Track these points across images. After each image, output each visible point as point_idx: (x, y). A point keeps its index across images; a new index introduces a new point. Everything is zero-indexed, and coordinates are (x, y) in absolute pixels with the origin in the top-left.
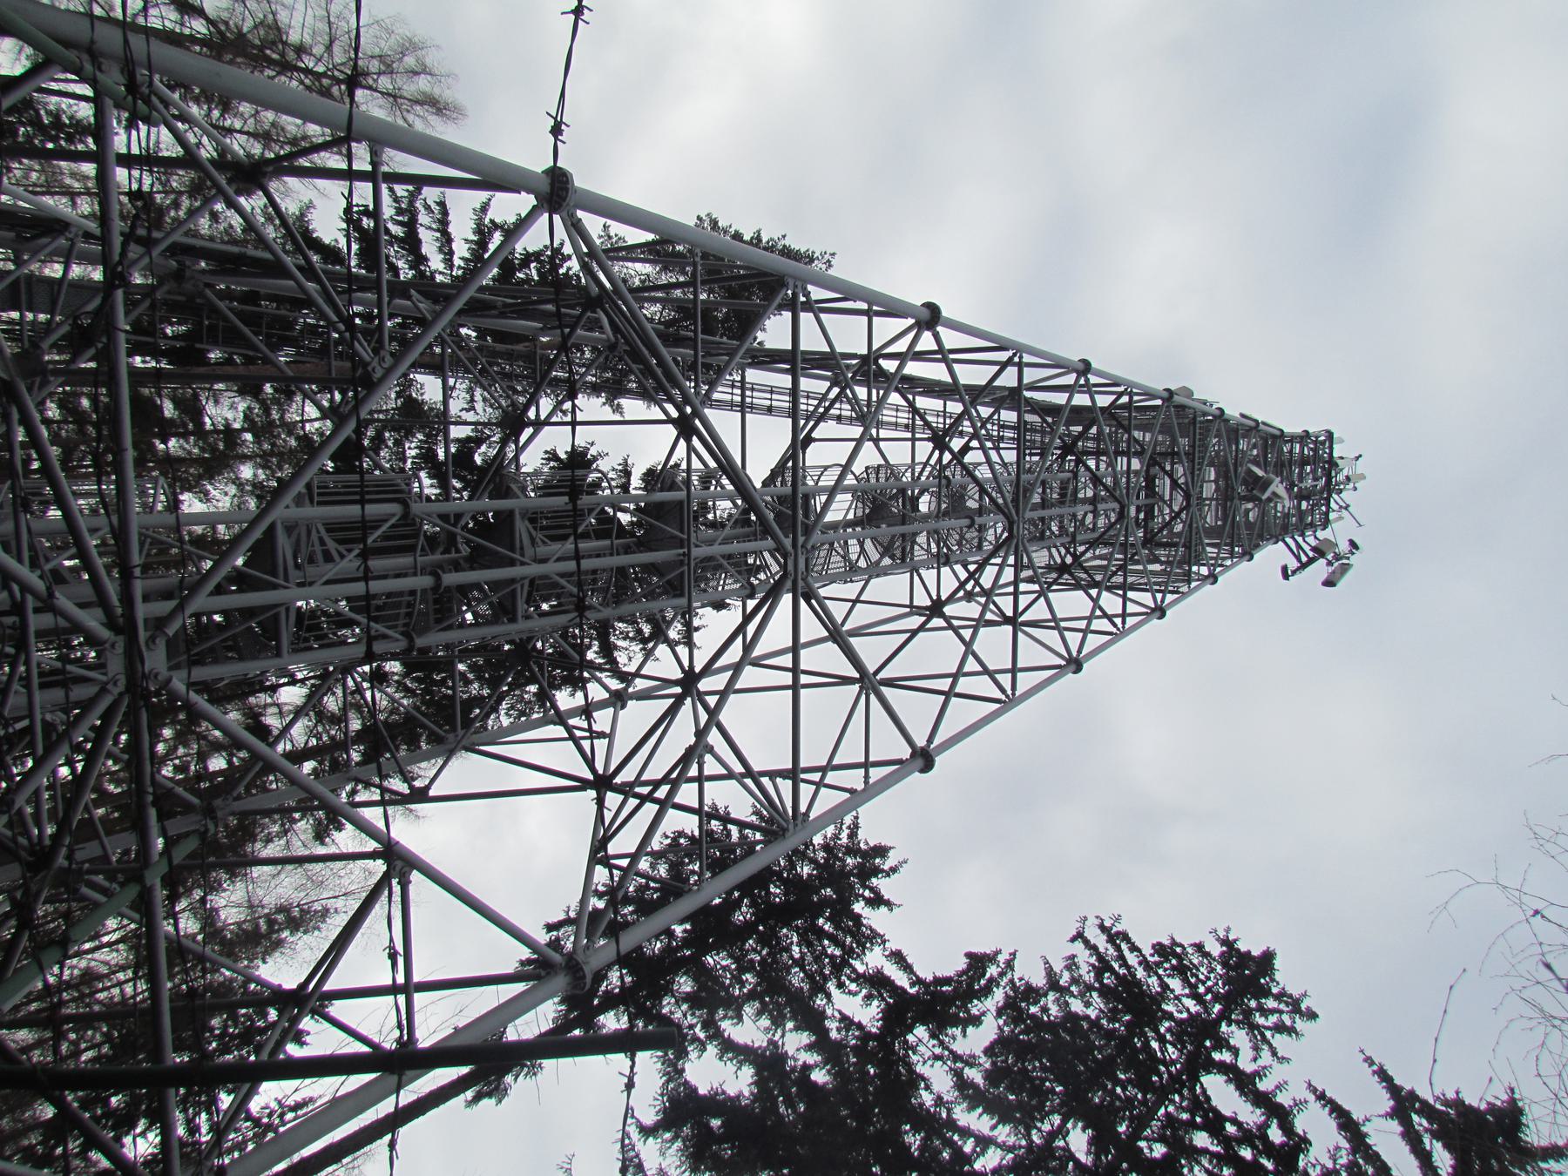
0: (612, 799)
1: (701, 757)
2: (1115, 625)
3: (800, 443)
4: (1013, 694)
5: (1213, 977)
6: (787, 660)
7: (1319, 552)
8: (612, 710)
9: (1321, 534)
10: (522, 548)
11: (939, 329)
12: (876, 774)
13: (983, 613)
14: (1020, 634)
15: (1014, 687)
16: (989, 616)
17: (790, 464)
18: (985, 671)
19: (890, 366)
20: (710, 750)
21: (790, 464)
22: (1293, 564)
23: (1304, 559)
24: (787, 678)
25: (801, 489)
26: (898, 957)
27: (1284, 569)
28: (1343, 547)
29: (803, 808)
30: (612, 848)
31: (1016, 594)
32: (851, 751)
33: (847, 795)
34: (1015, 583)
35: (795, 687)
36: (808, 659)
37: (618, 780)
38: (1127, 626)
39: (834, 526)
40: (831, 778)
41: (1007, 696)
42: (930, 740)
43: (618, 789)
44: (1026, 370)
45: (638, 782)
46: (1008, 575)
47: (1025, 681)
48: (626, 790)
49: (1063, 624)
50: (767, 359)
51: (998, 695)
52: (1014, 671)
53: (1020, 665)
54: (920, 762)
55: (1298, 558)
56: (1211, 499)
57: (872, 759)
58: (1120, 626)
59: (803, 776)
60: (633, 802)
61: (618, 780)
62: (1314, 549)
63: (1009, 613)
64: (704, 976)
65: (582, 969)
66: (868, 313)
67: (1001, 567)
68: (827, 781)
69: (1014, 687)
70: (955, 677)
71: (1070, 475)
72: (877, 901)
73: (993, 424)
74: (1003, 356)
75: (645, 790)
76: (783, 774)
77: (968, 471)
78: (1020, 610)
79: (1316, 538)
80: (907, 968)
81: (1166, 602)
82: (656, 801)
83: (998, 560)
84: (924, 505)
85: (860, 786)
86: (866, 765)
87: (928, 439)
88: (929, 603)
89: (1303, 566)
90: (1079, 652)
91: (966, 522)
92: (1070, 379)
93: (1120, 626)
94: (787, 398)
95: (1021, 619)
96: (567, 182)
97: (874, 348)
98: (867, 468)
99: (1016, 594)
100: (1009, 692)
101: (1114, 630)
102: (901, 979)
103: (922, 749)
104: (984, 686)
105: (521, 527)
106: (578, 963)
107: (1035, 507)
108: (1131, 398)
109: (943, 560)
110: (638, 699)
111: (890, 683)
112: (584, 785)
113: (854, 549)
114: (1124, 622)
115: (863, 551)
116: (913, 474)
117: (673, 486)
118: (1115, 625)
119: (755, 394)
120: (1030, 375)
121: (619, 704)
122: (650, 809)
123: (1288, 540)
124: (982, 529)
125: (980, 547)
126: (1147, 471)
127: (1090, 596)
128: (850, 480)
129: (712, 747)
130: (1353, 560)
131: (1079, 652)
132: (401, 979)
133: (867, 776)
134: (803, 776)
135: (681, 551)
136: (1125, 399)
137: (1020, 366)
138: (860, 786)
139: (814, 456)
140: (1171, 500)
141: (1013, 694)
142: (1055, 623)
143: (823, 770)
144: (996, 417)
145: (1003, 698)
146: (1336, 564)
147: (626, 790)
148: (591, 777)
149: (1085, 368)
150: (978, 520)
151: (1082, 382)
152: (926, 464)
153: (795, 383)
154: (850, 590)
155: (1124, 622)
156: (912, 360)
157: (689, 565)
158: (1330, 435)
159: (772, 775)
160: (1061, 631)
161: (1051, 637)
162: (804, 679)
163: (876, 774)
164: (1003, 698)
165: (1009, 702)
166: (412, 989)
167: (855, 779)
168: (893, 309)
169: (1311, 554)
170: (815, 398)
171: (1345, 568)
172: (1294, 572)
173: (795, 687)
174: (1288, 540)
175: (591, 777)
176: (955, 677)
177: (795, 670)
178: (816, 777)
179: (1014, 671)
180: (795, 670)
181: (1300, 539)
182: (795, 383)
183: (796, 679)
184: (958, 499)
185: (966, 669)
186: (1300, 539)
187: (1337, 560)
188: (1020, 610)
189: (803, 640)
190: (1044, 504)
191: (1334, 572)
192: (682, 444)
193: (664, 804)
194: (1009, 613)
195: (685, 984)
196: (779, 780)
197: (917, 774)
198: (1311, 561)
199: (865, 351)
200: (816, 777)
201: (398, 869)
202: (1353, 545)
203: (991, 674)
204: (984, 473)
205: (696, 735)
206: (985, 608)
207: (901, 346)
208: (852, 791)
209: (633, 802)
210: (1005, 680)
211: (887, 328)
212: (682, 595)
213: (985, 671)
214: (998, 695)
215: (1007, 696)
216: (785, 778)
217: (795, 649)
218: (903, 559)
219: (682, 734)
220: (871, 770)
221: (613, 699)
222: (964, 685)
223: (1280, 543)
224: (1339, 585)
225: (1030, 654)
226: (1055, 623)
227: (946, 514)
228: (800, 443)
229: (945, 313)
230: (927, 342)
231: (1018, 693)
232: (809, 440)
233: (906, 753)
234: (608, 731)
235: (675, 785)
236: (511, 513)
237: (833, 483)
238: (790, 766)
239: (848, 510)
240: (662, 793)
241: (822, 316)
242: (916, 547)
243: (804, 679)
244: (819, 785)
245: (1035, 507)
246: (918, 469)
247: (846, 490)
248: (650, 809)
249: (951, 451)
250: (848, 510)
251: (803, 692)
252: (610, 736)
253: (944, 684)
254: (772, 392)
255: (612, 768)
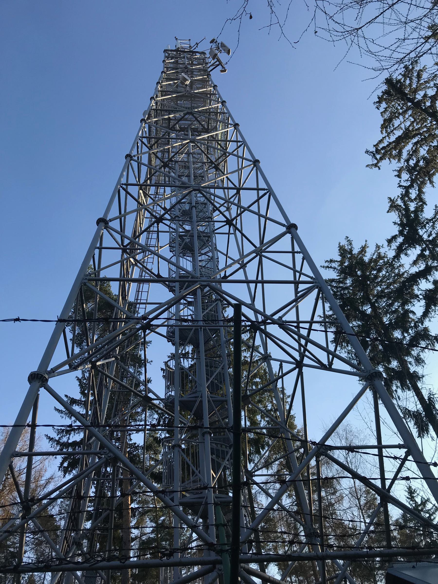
0: (306, 361)
1: (283, 321)
2: (241, 146)
3: (159, 279)
4: (267, 190)
5: (398, 105)
6: (252, 286)
7: (215, 56)
8: (272, 361)
9: (208, 55)
10: (196, 397)
11: (108, 219)
12: (297, 249)
13: (235, 204)
14: (244, 186)
15: (264, 189)
16: (236, 201)
17: (167, 283)
18: (257, 201)
19: (126, 242)
20: (281, 318)
21: (167, 283)
22: (220, 68)
23: (218, 63)
24: (259, 285)
25: (177, 279)
26: (390, 241)
27: (222, 71)
28: (214, 45)
29: (309, 279)
30: (325, 362)
31: (228, 188)
32: (287, 259)
33: (305, 261)
34: (224, 188)
35: (263, 282)
36: (252, 276)
37: (298, 358)
38: (241, 140)
39: (194, 266)
40: (298, 268)
41: (268, 192)
42: (284, 225)
43: (302, 359)
44: (130, 182)
45: (299, 351)
46: (219, 192)
47: (262, 185)
48: (302, 356)
49: (240, 167)
50: (124, 293)
51: (267, 196)
52: (258, 189)
53: (256, 187)
54: (293, 229)
55: (218, 65)
56: (192, 103)
57: (291, 250)
58: (241, 143)
59: (297, 279)
60: (307, 353)
61: (298, 358)
62: (214, 59)
63: (235, 191)
64: (393, 326)
65: (372, 374)
66: (101, 248)
67: (215, 196)
68: (299, 270)
69: (264, 189)
70: (260, 216)
71: (176, 164)
72: (363, 250)
73: (156, 197)
74: (123, 193)
75: (302, 349)
76: (296, 288)
77: (173, 207)
78: (233, 186)
79: (209, 58)
80: (394, 238)
81: (232, 123)
82: (306, 344)
83: (213, 197)
84: (188, 228)
85: (301, 255)
86: (293, 252)
87: (158, 225)
88: (228, 226)
89: (220, 64)
90: (250, 161)
91: (194, 209)
92: (135, 164)
93: (241, 143)
94: (141, 285)
95: (238, 186)
96: (35, 374)
97: (118, 246)
98: (171, 251)
99: (228, 188)
100: (266, 191)
101: (243, 146)
102: (400, 240)
103: (287, 229)
104: (264, 201)
105: (186, 397)
106: (369, 375)
107: (189, 180)
108: (144, 137)
109: (210, 220)
110: (267, 350)
111: (262, 242)
112: (300, 374)
113: (203, 257)
114: (240, 142)
115: (205, 254)
116: (173, 232)
117: (173, 333)
118: (241, 146)
119: (139, 298)
120: (132, 180)
121: (269, 358)
122: (310, 347)
123: (209, 70)
124: (197, 203)
125: (205, 204)
126: (177, 131)
127: (229, 156)
128: (174, 260)
129: (279, 317)
130: (219, 41)
131: (250, 161)
132: (376, 451)
133: (297, 252)
134: (297, 279)
135: (199, 329)
136: (145, 140)
137: (127, 185)
138: (301, 255)
139: (165, 274)
140: (191, 121)
141: (267, 190)
142: (239, 170)
143: (295, 271)
144: (152, 196)
145: (268, 194)
146: (221, 49)
147: (302, 356)
148: (297, 369)
149: (129, 157)
150: (194, 204)
151: (136, 158)
152: (170, 227)
153: (134, 281)
154: (222, 259)
155: (240, 142)
156: (124, 233)
157: (205, 326)
158: (165, 51)
159: (297, 292)
160: (242, 168)
161: (245, 173)
162: (260, 278)
163: (297, 249)
164: (268, 194)
165: (270, 192)
166: (380, 445)
167: (299, 257)
168: (99, 237)
169: (216, 60)
170: (142, 273)
171: (223, 45)
172: (223, 68)
173: (263, 282)
174: (209, 70)
175: (297, 369)
176: (260, 216)
177: (256, 282)
178: (298, 274)
179: (258, 189)
180: (256, 282)
181: (209, 65)
182: (134, 281)
183: (260, 282)
184: (186, 213)
185: (257, 211)
186: (209, 65)
187: (219, 48)
188: (233, 186)
189: (244, 278)
190: (188, 176)
191: (224, 50)
192: (158, 330)
193: (308, 340)
194: (235, 191)
195: (397, 334)
196: (299, 290)
197: (298, 231)
198: (218, 60)
199: (120, 251)
200: (298, 274)
201: (323, 451)
202: (212, 41)
203: (259, 198)
204: (174, 200)
205: (274, 324)
206: (233, 203)
207: (118, 237)
208: (303, 259)
209: (307, 353)
210: (261, 193)
211: (108, 241)
212: (219, 329)
213: (257, 201)
214: (267, 196)
215: (268, 192)
216: (298, 287)
217: (248, 282)
218: (209, 237)
219: (273, 329)
220: (296, 250)
221: (267, 360)
222: (263, 212)
223: (211, 73)
224: (229, 47)
225: (251, 183)
226: (239, 170)
227: (191, 218)
228: (159, 279)
229: (101, 216)
230: (115, 224)
231: (266, 188)
232: (159, 276)
233: (288, 236)
234: (280, 363)
235: (301, 336)
236: (180, 402)
237: (181, 265)
238: (293, 285)
239: (187, 260)
240: (303, 342)
241: (102, 267)
242: (206, 231)
243: (260, 278)
244: (301, 273)
245: (189, 180)
246: (171, 230)
247: (178, 260)
248: (310, 347)
249: (164, 214)
250: (187, 260)
251: (265, 279)
252: (281, 362)
253: (263, 220)
254: (139, 291)
255: (293, 361)
